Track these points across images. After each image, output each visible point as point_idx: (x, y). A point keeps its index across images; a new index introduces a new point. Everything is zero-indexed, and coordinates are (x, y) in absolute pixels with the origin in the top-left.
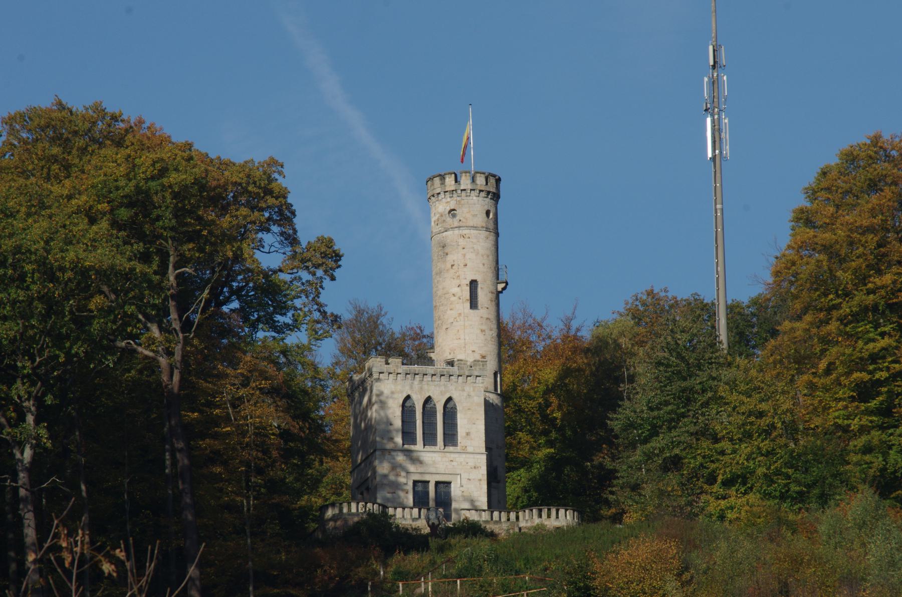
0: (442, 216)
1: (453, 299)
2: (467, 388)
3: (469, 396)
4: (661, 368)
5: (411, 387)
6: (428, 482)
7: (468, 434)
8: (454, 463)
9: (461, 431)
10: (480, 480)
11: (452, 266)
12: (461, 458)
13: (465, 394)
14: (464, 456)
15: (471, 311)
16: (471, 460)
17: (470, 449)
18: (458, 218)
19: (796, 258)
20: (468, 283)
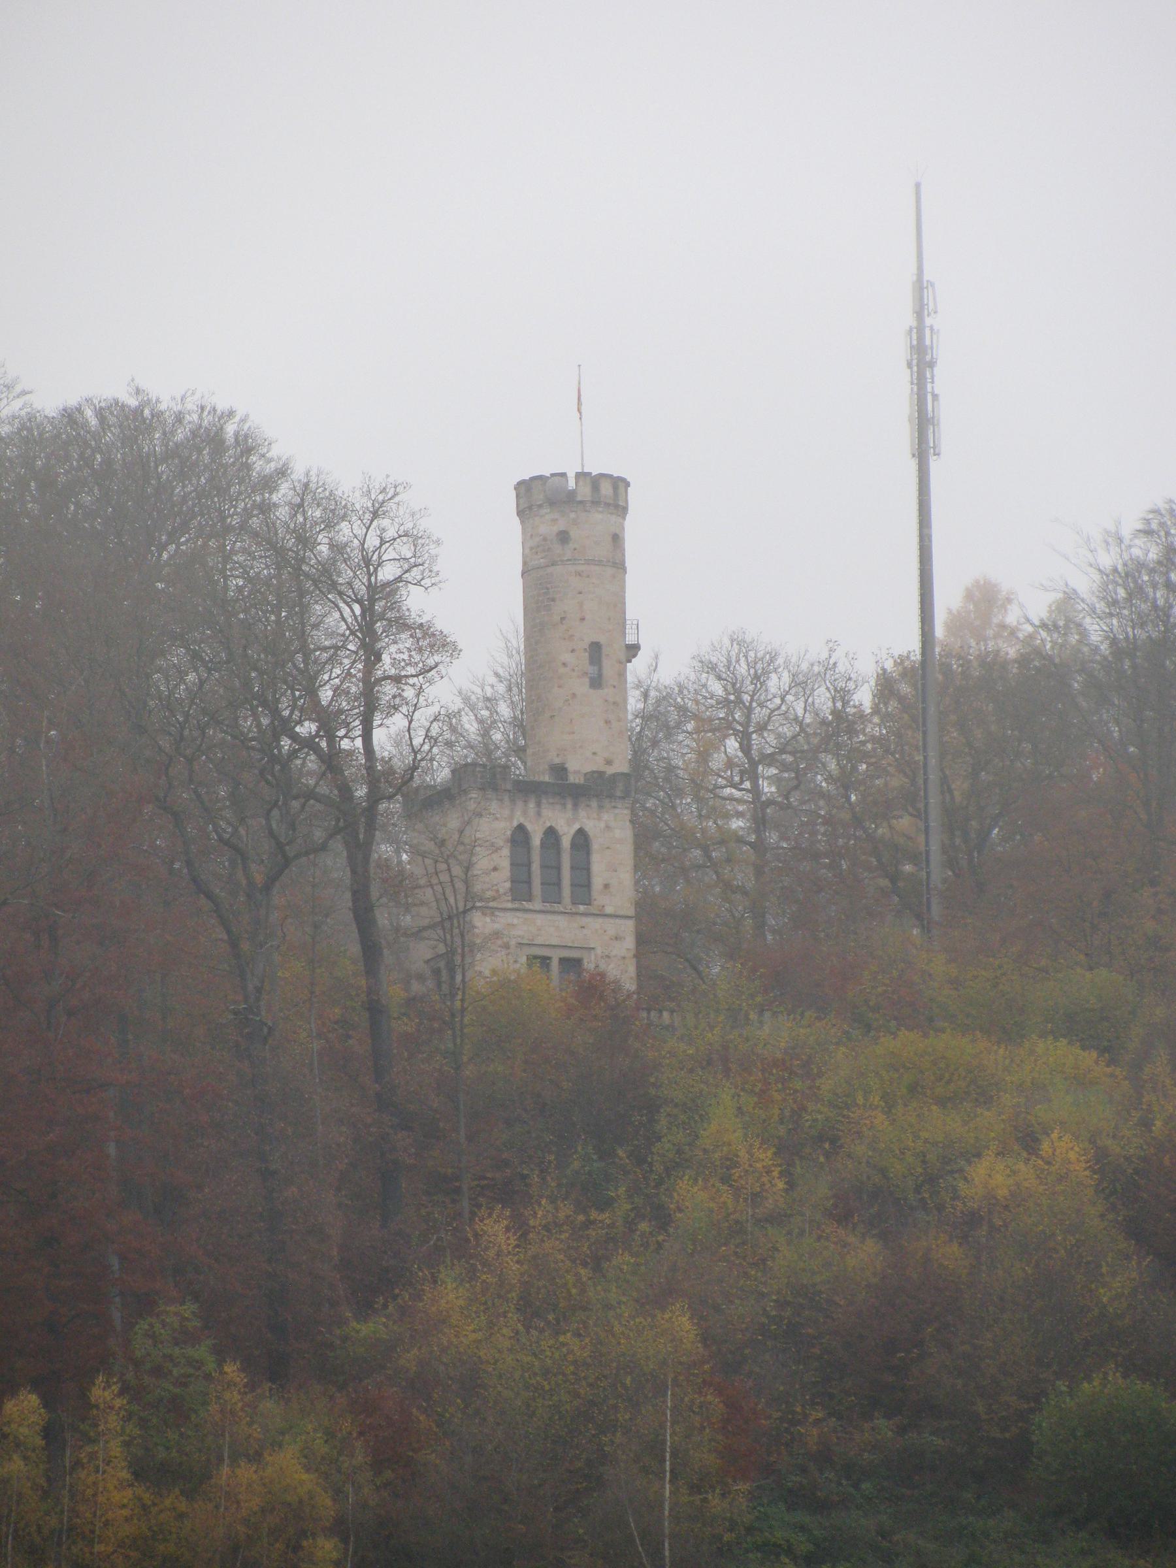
0: (545, 539)
1: (562, 670)
2: (605, 817)
3: (608, 827)
4: (623, 1260)
5: (525, 813)
6: (549, 958)
7: (606, 886)
8: (585, 931)
9: (598, 879)
10: (624, 958)
11: (563, 619)
12: (595, 924)
13: (602, 825)
14: (600, 920)
15: (591, 691)
16: (612, 926)
17: (609, 910)
18: (571, 545)
19: (116, 1408)
20: (587, 647)
